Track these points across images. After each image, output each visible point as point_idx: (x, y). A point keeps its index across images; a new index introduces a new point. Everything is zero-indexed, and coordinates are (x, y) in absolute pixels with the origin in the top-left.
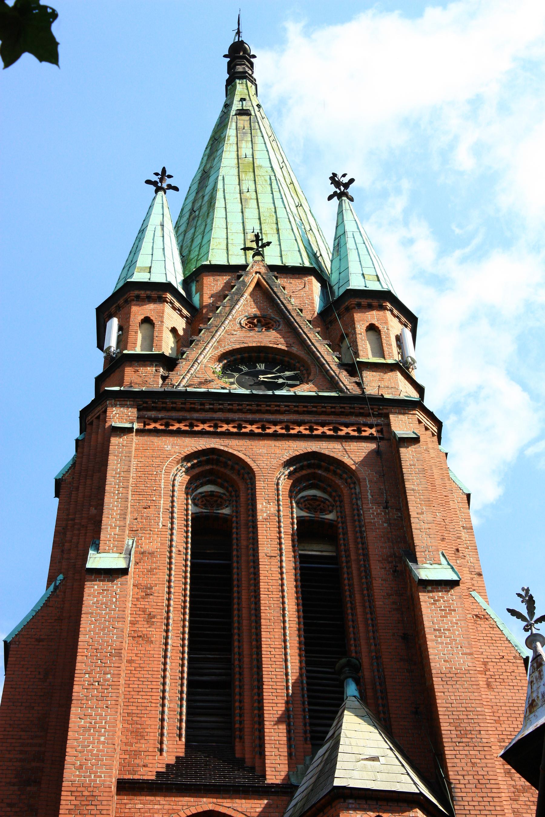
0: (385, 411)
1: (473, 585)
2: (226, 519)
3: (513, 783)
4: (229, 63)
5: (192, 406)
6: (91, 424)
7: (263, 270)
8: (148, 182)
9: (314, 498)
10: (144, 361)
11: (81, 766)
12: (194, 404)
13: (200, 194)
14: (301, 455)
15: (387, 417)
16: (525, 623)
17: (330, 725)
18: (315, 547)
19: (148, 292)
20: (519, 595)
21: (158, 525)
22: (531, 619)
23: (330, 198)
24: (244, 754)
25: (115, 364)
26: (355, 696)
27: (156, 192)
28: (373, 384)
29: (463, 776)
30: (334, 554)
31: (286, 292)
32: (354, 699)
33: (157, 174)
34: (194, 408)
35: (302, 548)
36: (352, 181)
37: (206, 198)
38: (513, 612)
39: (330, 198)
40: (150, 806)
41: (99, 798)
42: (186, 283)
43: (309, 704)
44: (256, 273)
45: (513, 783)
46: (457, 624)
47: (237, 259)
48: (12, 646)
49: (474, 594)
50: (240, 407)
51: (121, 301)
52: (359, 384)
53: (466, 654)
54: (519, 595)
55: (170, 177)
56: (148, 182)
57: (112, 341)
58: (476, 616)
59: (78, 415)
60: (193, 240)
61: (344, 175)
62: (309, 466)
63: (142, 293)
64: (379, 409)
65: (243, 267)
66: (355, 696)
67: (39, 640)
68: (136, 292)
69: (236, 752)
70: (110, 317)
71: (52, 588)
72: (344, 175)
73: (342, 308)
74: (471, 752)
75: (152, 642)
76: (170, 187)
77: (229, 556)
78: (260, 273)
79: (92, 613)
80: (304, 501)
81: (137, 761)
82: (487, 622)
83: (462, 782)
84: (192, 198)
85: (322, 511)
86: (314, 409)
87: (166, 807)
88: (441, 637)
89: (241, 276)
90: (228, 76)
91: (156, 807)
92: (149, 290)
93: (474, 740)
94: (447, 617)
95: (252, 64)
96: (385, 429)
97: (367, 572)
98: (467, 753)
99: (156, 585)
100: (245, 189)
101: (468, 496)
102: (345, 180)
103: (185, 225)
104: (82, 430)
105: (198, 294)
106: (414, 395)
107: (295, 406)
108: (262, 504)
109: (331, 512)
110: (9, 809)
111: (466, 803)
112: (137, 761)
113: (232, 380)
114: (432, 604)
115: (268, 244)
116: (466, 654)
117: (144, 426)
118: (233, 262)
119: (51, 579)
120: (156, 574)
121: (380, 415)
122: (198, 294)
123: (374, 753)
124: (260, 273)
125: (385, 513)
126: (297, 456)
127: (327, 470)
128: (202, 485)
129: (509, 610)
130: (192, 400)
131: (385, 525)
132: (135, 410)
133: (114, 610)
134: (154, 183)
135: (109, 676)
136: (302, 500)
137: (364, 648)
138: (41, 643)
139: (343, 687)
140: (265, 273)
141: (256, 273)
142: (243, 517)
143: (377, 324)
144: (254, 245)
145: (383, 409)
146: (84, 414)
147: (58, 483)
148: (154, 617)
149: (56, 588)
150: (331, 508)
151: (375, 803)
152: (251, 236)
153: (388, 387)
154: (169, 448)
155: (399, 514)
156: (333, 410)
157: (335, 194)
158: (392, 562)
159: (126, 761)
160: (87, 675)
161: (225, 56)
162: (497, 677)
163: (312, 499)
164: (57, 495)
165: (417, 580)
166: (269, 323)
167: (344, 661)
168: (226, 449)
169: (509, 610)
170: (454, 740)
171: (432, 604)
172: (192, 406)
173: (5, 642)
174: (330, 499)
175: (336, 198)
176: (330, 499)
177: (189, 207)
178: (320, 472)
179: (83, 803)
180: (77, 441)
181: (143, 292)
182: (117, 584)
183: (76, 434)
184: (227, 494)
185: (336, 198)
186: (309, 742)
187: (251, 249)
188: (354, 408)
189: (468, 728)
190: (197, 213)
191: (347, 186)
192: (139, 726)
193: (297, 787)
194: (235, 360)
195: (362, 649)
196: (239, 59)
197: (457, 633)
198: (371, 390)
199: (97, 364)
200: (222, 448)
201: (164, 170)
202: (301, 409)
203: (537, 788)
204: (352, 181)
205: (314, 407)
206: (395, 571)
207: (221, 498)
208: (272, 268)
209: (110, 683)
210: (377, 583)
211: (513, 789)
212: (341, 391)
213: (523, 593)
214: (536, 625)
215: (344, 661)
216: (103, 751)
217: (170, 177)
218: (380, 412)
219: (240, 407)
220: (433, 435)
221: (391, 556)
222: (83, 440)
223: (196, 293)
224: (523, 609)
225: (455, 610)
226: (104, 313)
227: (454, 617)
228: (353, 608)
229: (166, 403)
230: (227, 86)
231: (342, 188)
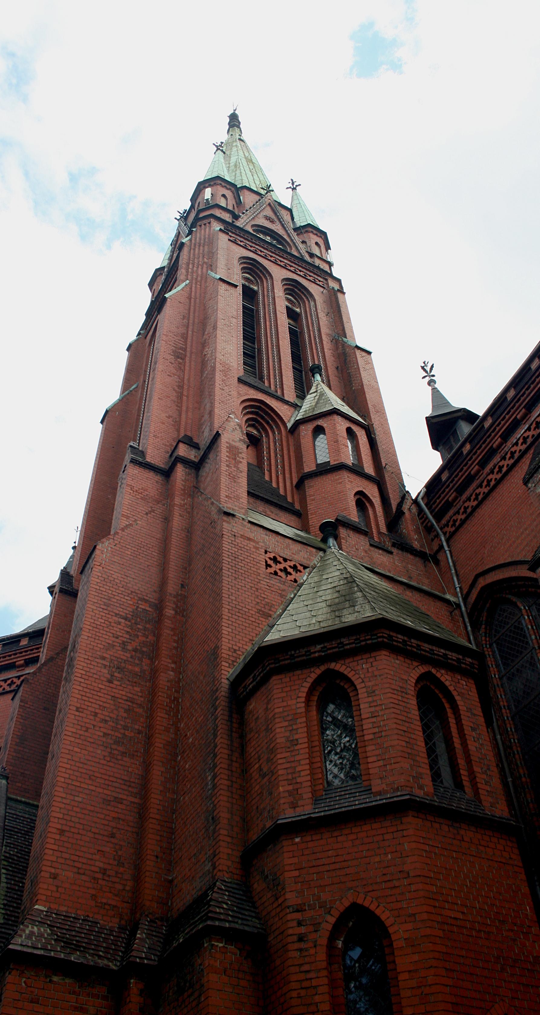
51: (212, 183)
62: (292, 285)
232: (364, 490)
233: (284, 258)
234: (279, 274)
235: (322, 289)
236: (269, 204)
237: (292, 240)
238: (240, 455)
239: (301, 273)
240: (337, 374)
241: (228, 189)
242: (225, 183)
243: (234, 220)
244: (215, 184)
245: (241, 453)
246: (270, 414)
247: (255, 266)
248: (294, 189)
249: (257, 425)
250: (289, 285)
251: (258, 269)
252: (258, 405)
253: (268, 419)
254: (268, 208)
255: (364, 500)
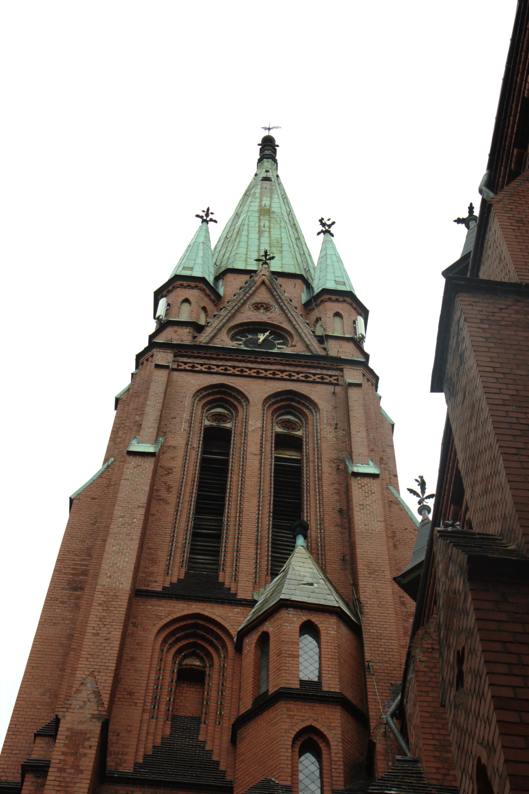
0: (341, 367)
1: (390, 482)
2: (228, 432)
3: (406, 610)
4: (261, 149)
5: (211, 356)
6: (142, 364)
7: (267, 274)
8: (198, 216)
9: (289, 421)
10: (182, 326)
11: (110, 577)
12: (212, 354)
13: (232, 228)
14: (281, 391)
15: (342, 370)
16: (419, 499)
17: (285, 562)
18: (287, 453)
19: (189, 283)
20: (417, 480)
21: (181, 429)
22: (423, 495)
23: (319, 234)
24: (224, 580)
25: (163, 325)
26: (302, 546)
27: (202, 222)
28: (334, 349)
29: (370, 599)
30: (299, 458)
31: (282, 289)
32: (302, 548)
33: (204, 211)
34: (212, 357)
35: (278, 452)
36: (333, 223)
37: (236, 230)
38: (411, 491)
39: (319, 234)
40: (157, 608)
41: (120, 597)
42: (217, 279)
43: (272, 552)
44: (263, 275)
45: (406, 610)
46: (375, 502)
47: (253, 266)
48: (74, 501)
49: (390, 487)
50: (244, 359)
51: (170, 288)
52: (325, 349)
53: (379, 521)
54: (417, 480)
55: (212, 213)
56: (198, 216)
57: (161, 310)
58: (391, 501)
59: (135, 358)
60: (224, 255)
61: (329, 220)
62: (286, 400)
63: (185, 283)
64: (338, 365)
65: (255, 272)
66: (302, 546)
67: (93, 499)
68: (181, 282)
69: (220, 578)
70: (162, 297)
71: (106, 464)
72: (329, 220)
73: (318, 302)
74: (377, 584)
75: (169, 503)
76: (211, 220)
77: (228, 455)
78: (265, 275)
79: (128, 479)
80: (282, 422)
81: (151, 579)
82: (398, 506)
83: (369, 602)
84: (227, 230)
85: (293, 429)
86: (293, 363)
87: (168, 609)
88: (363, 509)
89: (253, 276)
90: (259, 157)
91: (160, 608)
92: (190, 281)
93: (379, 576)
94: (368, 497)
95: (276, 150)
96: (340, 378)
97: (319, 468)
98: (374, 584)
99: (175, 468)
100: (262, 224)
101: (393, 426)
102: (329, 223)
103: (221, 246)
104: (137, 367)
105: (223, 287)
106: (363, 360)
107: (281, 360)
108: (252, 421)
109: (299, 430)
110: (61, 605)
111: (370, 616)
112: (151, 579)
113: (240, 343)
114: (359, 488)
115: (273, 258)
116: (379, 521)
117: (178, 367)
118: (249, 268)
119: (106, 460)
120: (176, 460)
121: (337, 369)
122: (223, 287)
123: (310, 581)
124: (265, 275)
125: (335, 432)
126: (279, 392)
127: (299, 402)
128: (214, 408)
129: (408, 489)
130: (211, 352)
131: (334, 439)
132: (171, 355)
133: (143, 478)
134: (202, 217)
135: (135, 520)
136: (280, 422)
137: (313, 517)
138: (94, 501)
139: (295, 539)
140: (268, 276)
141: (263, 275)
142: (239, 429)
143: (341, 312)
144: (264, 258)
145: (339, 366)
146: (139, 357)
147: (117, 400)
148: (172, 488)
149: (108, 466)
150: (299, 428)
151: (307, 611)
152: (262, 253)
153: (344, 352)
154: (193, 381)
155: (344, 433)
156: (306, 364)
157: (322, 231)
158: (336, 463)
159: (143, 578)
160: (121, 519)
161: (259, 145)
162: (401, 541)
163: (287, 422)
164: (116, 409)
165: (350, 472)
166: (269, 308)
167: (297, 523)
168: (232, 385)
169: (408, 489)
170: (366, 575)
171: (359, 488)
172: (211, 356)
173: (70, 498)
174: (299, 422)
175: (322, 234)
176: (299, 422)
177: (225, 236)
178: (294, 404)
179: (109, 600)
180: (132, 374)
181: (185, 282)
182: (147, 462)
183: (133, 370)
184: (230, 414)
185: (322, 234)
186: (269, 575)
187: (262, 260)
188: (320, 364)
189: (376, 569)
190: (229, 239)
191: (329, 226)
192: (155, 557)
193: (257, 602)
194: (244, 330)
195: (311, 514)
196: (268, 147)
197: (375, 507)
198: (333, 353)
199: (152, 327)
200: (229, 384)
201: (208, 209)
202: (284, 362)
203: (415, 601)
204: (333, 223)
205: (293, 361)
206: (338, 469)
207: (226, 416)
208: (274, 273)
209: (136, 524)
210: (325, 476)
211: (405, 614)
212: (312, 352)
213: (419, 480)
214: (425, 500)
215: (297, 523)
216: (126, 567)
217: (212, 213)
218: (338, 367)
219: (244, 359)
220: (372, 385)
221: (336, 459)
222: (136, 374)
223: (222, 286)
224: (418, 490)
225: (374, 493)
226: (158, 294)
227: (374, 497)
228: (308, 491)
229: (193, 353)
230: (258, 163)
231: (327, 228)
232: (314, 724)
233: (271, 364)
234: (257, 391)
235: (331, 388)
236: (263, 283)
237: (294, 327)
238: (87, 743)
239: (284, 375)
240: (339, 521)
241: (193, 288)
242: (335, 295)
243: (196, 334)
244: (174, 287)
245: (88, 739)
246: (212, 630)
247: (225, 393)
248: (205, 221)
249: (198, 651)
250: (274, 403)
251: (230, 395)
252: (193, 621)
253: (211, 638)
254: (263, 290)
255: (315, 738)
